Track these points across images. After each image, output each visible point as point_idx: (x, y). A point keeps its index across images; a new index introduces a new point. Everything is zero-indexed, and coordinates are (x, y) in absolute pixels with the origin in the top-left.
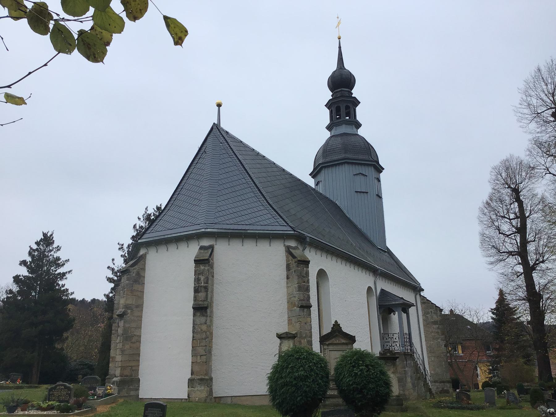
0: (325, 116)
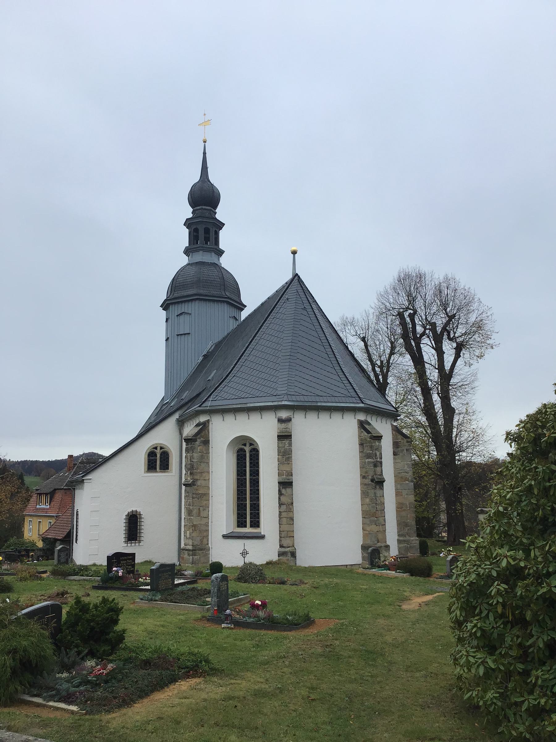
0: (183, 237)
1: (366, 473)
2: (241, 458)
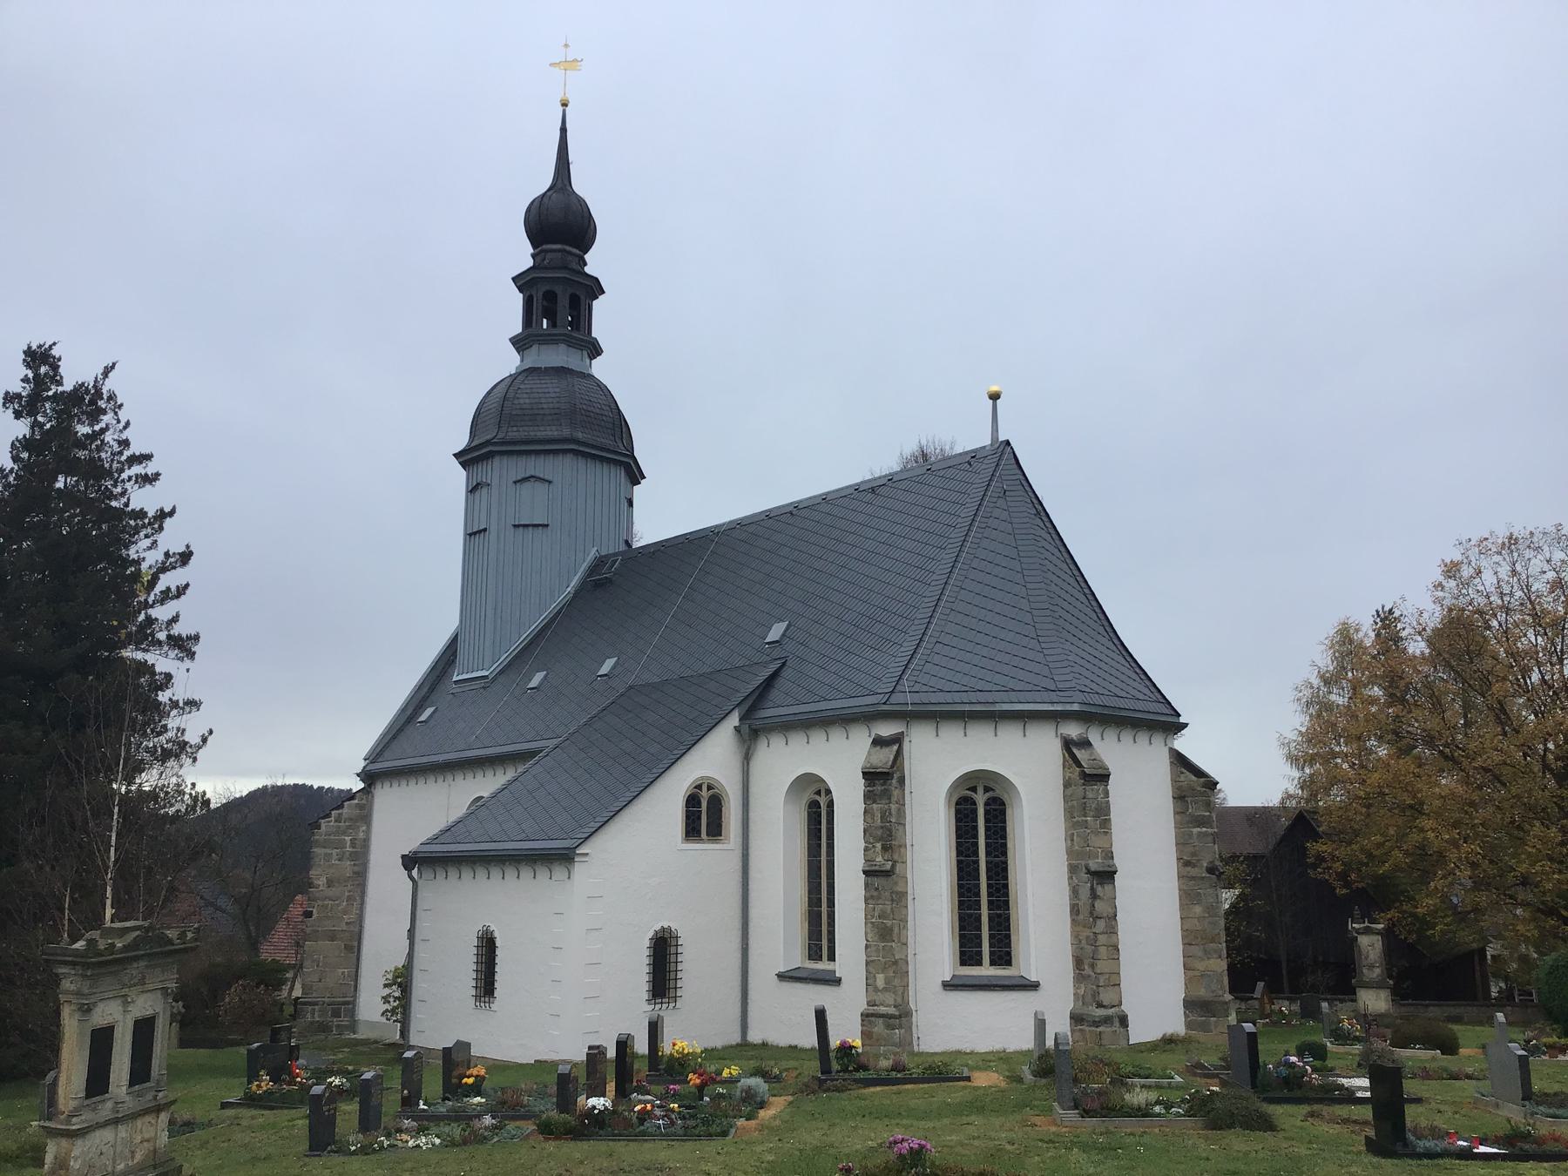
0: (510, 311)
1: (1194, 854)
2: (967, 816)
